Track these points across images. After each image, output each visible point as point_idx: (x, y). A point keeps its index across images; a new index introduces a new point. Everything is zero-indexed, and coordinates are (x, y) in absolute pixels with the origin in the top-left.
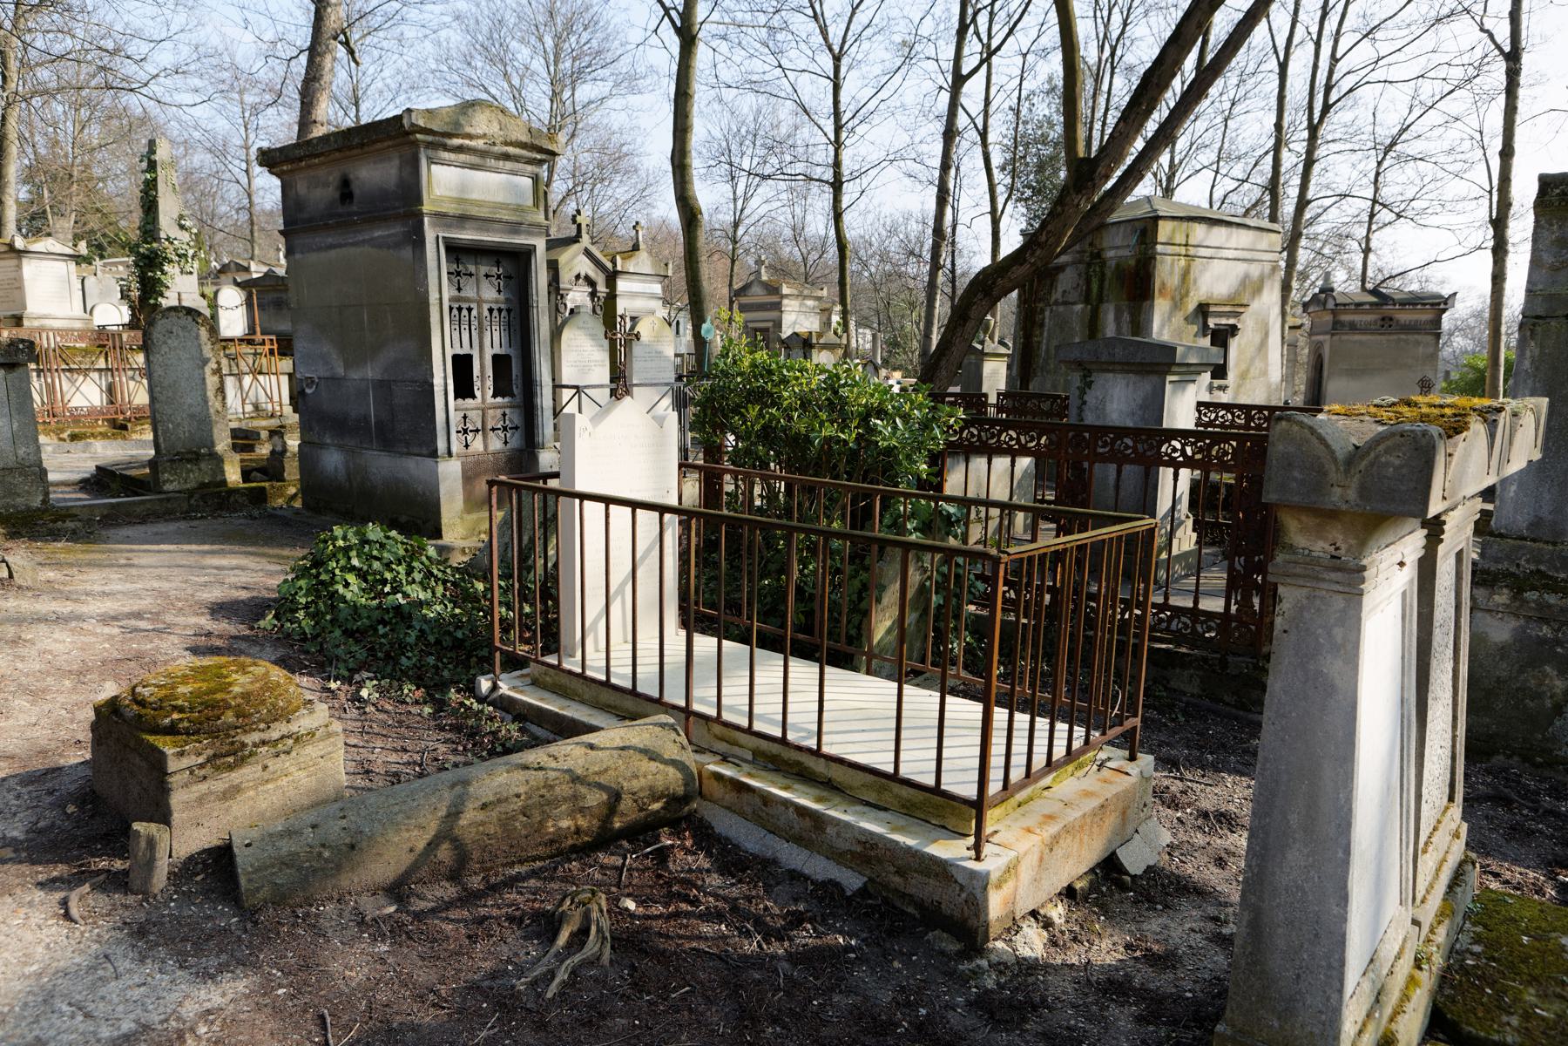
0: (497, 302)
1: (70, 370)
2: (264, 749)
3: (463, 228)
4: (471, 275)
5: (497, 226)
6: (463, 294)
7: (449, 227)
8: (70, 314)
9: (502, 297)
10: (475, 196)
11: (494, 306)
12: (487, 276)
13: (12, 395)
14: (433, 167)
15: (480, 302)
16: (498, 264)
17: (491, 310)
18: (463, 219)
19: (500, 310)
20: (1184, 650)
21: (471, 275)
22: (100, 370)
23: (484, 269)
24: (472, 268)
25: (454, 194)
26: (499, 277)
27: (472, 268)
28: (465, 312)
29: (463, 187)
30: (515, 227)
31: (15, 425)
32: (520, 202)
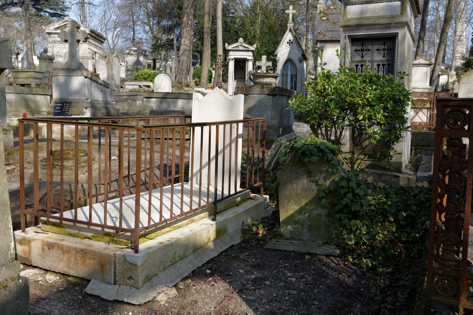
0: (382, 61)
1: (416, 108)
2: (57, 167)
3: (359, 30)
4: (369, 50)
5: (377, 27)
6: (364, 59)
7: (353, 30)
8: (425, 86)
9: (385, 59)
10: (368, 15)
11: (385, 63)
12: (378, 50)
13: (273, 104)
14: (348, 7)
15: (372, 62)
16: (384, 44)
17: (378, 65)
18: (359, 26)
19: (384, 65)
20: (426, 279)
21: (369, 50)
22: (428, 108)
23: (376, 47)
24: (370, 47)
25: (357, 16)
26: (384, 50)
27: (370, 47)
28: (359, 67)
29: (362, 12)
30: (387, 26)
31: (273, 114)
32: (392, 13)
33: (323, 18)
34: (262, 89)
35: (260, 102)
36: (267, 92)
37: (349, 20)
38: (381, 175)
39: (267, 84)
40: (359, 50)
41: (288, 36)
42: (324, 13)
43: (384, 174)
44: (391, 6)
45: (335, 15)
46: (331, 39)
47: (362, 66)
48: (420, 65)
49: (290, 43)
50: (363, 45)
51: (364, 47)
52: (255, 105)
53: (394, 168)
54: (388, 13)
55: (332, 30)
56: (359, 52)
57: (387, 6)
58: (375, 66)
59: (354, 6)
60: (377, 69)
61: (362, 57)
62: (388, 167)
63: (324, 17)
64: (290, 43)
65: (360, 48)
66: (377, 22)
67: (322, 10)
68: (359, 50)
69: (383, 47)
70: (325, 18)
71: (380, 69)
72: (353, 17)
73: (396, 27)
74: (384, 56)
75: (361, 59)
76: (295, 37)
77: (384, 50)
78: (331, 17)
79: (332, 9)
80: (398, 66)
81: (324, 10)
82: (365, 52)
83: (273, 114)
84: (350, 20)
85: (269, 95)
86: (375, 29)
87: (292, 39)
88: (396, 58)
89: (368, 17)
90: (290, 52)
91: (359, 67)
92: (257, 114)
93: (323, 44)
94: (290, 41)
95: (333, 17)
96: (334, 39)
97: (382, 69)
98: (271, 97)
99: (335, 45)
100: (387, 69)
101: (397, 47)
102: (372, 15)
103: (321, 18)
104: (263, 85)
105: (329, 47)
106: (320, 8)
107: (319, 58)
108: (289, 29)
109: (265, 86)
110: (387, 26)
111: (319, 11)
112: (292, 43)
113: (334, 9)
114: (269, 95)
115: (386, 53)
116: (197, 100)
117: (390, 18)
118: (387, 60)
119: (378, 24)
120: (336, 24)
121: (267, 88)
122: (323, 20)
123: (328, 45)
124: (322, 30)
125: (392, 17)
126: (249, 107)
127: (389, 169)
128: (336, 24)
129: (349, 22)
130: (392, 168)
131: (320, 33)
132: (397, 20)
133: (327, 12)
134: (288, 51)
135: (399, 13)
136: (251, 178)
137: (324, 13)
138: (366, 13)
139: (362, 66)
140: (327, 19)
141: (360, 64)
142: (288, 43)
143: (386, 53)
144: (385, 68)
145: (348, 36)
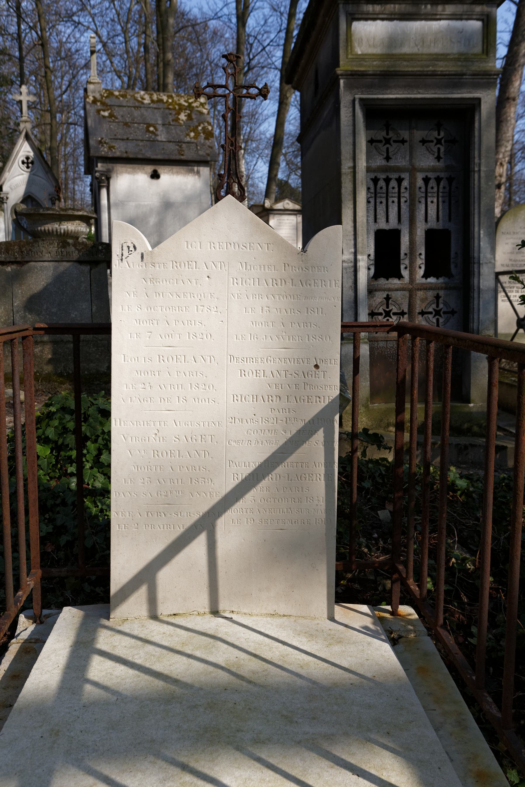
0: (433, 170)
4: (403, 142)
6: (392, 163)
7: (370, 87)
9: (441, 164)
10: (406, 50)
11: (442, 175)
12: (423, 142)
15: (413, 170)
16: (438, 127)
17: (426, 180)
18: (386, 77)
19: (438, 180)
21: (403, 142)
23: (419, 134)
24: (405, 134)
25: (378, 51)
26: (439, 142)
27: (405, 134)
28: (382, 183)
29: (392, 41)
30: (455, 80)
32: (463, 49)
33: (102, 113)
34: (64, 247)
35: (59, 280)
36: (76, 255)
37: (363, 58)
38: (466, 447)
39: (67, 235)
40: (380, 141)
41: (24, 150)
42: (103, 103)
43: (473, 446)
44: (461, 32)
45: (124, 109)
46: (125, 155)
47: (387, 181)
48: (285, 211)
49: (27, 162)
50: (388, 128)
51: (391, 134)
52: (45, 289)
53: (480, 426)
54: (455, 49)
55: (125, 137)
56: (380, 145)
57: (449, 30)
58: (420, 183)
59: (369, 22)
60: (423, 189)
61: (388, 158)
62: (466, 426)
63: (104, 111)
64: (27, 162)
65: (381, 135)
66: (431, 68)
67: (98, 96)
68: (380, 141)
69: (435, 133)
70: (106, 114)
71: (429, 190)
72: (371, 51)
73: (477, 86)
74: (438, 158)
75: (384, 163)
76: (38, 151)
77: (439, 142)
78: (118, 112)
79: (117, 97)
80: (483, 181)
81: (102, 96)
82: (395, 145)
83: (94, 309)
84: (363, 59)
85: (80, 262)
86: (427, 87)
87: (31, 154)
88: (477, 160)
89: (405, 54)
90: (30, 183)
91: (382, 183)
92: (54, 310)
93: (110, 166)
94: (28, 158)
95: (121, 113)
96: (131, 156)
97: (435, 189)
98: (86, 268)
99: (134, 169)
100: (447, 189)
101: (476, 133)
102: (415, 50)
103: (98, 111)
104: (64, 239)
105: (122, 173)
106: (94, 91)
107: (104, 192)
108: (24, 134)
109: (70, 241)
110: (455, 80)
111: (91, 98)
112: (32, 163)
113: (122, 96)
114: (80, 262)
115: (442, 150)
116: (136, 256)
117: (458, 60)
118: (447, 168)
119: (434, 74)
120: (129, 127)
121: (74, 245)
122: (104, 117)
123: (119, 167)
124: (104, 136)
125: (464, 58)
126: (31, 293)
127: (469, 430)
128: (129, 127)
129: (361, 66)
130: (476, 429)
131: (100, 142)
132: (477, 67)
133: (108, 101)
134: (26, 180)
135: (478, 49)
136: (422, 564)
137: (103, 103)
138: (402, 45)
139: (387, 181)
140: (111, 115)
141: (382, 176)
142: (23, 163)
143: (442, 150)
144: (441, 186)
145: (361, 100)
